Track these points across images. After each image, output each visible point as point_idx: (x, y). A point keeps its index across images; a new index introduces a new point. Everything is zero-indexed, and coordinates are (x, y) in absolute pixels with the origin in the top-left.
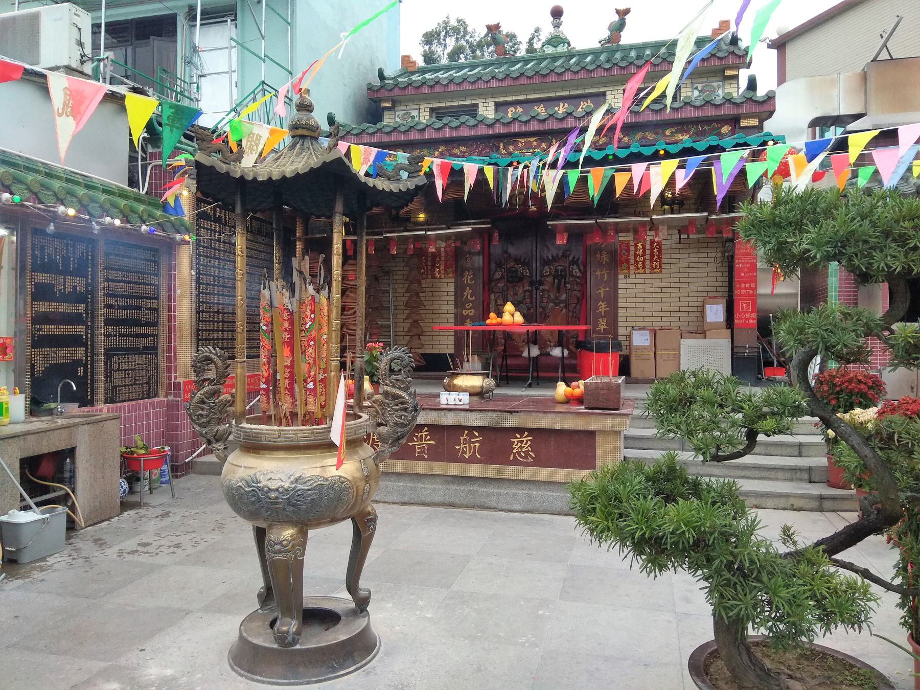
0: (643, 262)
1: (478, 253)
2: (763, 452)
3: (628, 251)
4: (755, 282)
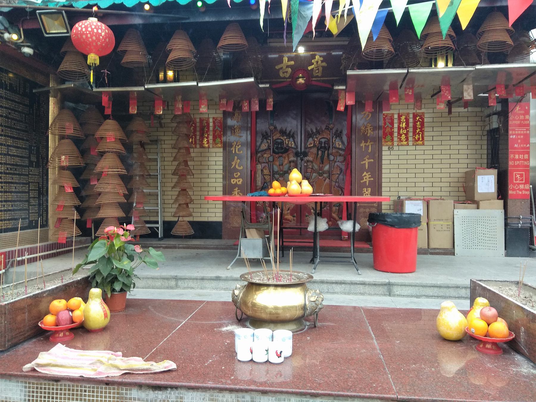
0: (406, 134)
3: (392, 123)
4: (528, 153)
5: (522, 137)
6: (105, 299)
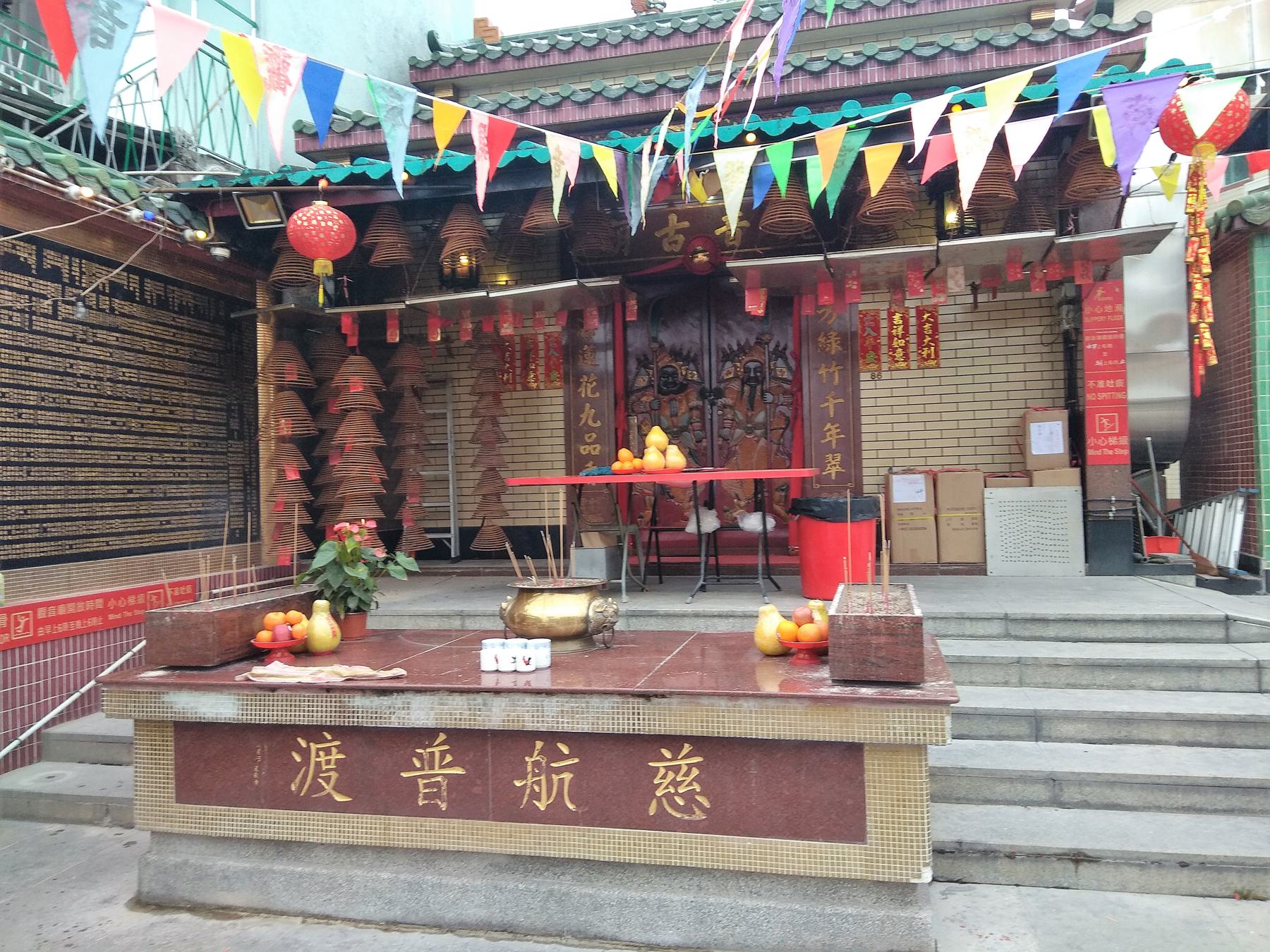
0: (905, 348)
1: (604, 347)
2: (1215, 740)
3: (877, 329)
4: (1123, 376)
5: (1110, 346)
6: (335, 615)
